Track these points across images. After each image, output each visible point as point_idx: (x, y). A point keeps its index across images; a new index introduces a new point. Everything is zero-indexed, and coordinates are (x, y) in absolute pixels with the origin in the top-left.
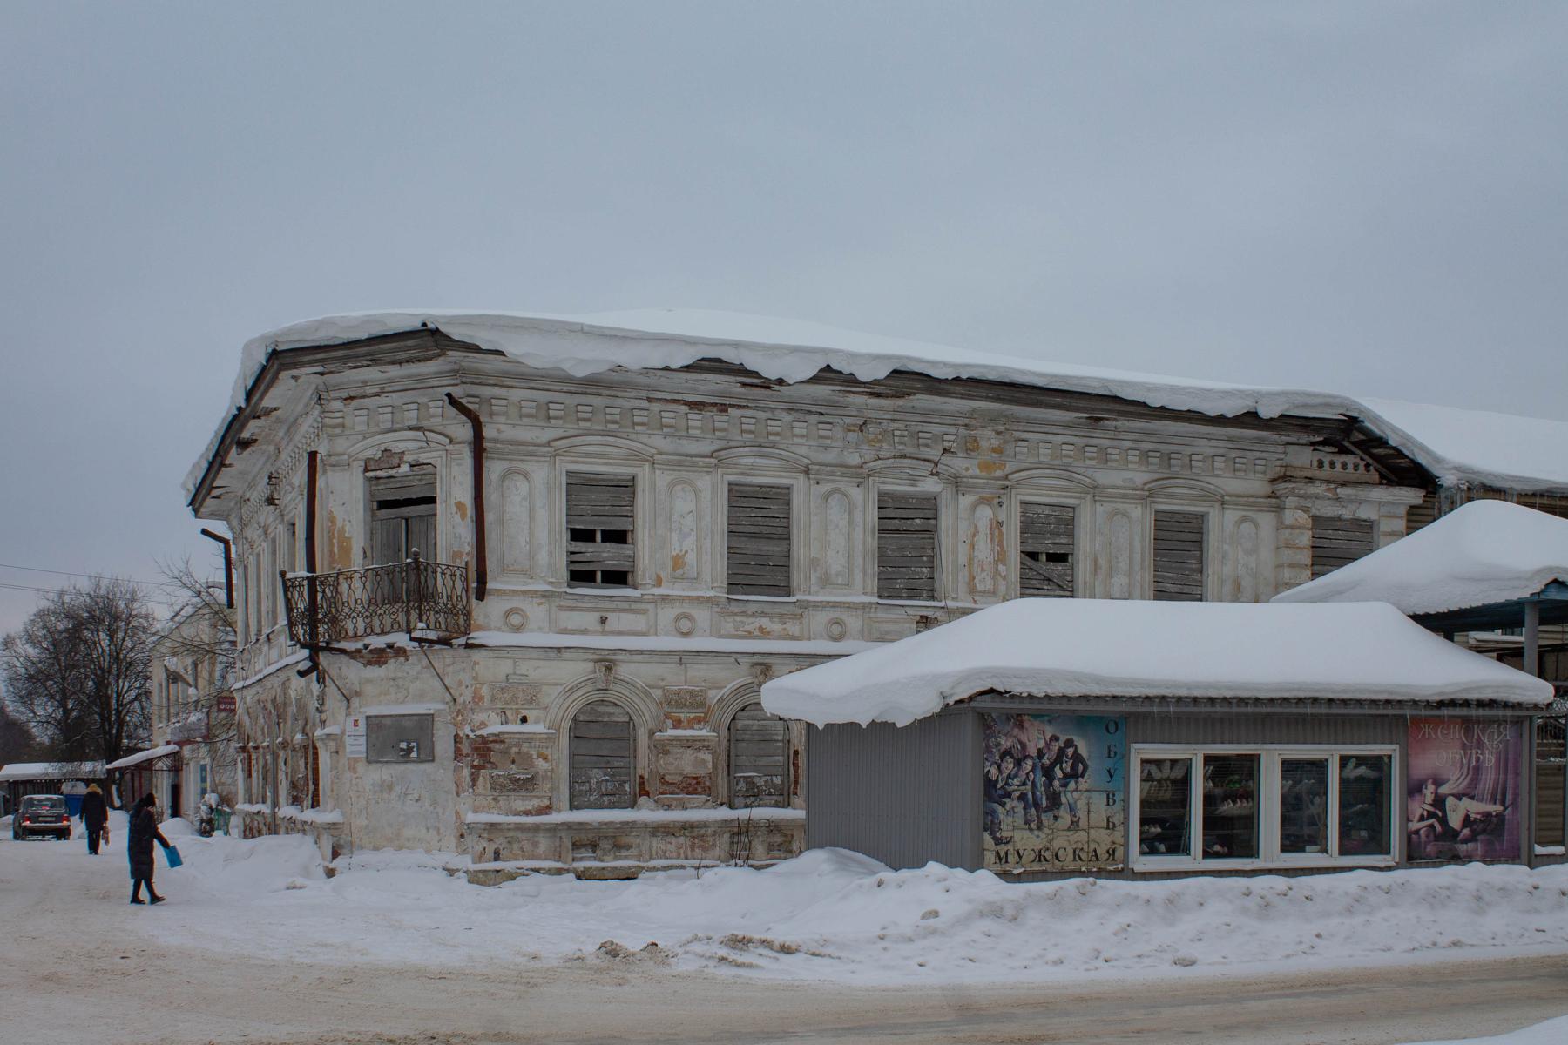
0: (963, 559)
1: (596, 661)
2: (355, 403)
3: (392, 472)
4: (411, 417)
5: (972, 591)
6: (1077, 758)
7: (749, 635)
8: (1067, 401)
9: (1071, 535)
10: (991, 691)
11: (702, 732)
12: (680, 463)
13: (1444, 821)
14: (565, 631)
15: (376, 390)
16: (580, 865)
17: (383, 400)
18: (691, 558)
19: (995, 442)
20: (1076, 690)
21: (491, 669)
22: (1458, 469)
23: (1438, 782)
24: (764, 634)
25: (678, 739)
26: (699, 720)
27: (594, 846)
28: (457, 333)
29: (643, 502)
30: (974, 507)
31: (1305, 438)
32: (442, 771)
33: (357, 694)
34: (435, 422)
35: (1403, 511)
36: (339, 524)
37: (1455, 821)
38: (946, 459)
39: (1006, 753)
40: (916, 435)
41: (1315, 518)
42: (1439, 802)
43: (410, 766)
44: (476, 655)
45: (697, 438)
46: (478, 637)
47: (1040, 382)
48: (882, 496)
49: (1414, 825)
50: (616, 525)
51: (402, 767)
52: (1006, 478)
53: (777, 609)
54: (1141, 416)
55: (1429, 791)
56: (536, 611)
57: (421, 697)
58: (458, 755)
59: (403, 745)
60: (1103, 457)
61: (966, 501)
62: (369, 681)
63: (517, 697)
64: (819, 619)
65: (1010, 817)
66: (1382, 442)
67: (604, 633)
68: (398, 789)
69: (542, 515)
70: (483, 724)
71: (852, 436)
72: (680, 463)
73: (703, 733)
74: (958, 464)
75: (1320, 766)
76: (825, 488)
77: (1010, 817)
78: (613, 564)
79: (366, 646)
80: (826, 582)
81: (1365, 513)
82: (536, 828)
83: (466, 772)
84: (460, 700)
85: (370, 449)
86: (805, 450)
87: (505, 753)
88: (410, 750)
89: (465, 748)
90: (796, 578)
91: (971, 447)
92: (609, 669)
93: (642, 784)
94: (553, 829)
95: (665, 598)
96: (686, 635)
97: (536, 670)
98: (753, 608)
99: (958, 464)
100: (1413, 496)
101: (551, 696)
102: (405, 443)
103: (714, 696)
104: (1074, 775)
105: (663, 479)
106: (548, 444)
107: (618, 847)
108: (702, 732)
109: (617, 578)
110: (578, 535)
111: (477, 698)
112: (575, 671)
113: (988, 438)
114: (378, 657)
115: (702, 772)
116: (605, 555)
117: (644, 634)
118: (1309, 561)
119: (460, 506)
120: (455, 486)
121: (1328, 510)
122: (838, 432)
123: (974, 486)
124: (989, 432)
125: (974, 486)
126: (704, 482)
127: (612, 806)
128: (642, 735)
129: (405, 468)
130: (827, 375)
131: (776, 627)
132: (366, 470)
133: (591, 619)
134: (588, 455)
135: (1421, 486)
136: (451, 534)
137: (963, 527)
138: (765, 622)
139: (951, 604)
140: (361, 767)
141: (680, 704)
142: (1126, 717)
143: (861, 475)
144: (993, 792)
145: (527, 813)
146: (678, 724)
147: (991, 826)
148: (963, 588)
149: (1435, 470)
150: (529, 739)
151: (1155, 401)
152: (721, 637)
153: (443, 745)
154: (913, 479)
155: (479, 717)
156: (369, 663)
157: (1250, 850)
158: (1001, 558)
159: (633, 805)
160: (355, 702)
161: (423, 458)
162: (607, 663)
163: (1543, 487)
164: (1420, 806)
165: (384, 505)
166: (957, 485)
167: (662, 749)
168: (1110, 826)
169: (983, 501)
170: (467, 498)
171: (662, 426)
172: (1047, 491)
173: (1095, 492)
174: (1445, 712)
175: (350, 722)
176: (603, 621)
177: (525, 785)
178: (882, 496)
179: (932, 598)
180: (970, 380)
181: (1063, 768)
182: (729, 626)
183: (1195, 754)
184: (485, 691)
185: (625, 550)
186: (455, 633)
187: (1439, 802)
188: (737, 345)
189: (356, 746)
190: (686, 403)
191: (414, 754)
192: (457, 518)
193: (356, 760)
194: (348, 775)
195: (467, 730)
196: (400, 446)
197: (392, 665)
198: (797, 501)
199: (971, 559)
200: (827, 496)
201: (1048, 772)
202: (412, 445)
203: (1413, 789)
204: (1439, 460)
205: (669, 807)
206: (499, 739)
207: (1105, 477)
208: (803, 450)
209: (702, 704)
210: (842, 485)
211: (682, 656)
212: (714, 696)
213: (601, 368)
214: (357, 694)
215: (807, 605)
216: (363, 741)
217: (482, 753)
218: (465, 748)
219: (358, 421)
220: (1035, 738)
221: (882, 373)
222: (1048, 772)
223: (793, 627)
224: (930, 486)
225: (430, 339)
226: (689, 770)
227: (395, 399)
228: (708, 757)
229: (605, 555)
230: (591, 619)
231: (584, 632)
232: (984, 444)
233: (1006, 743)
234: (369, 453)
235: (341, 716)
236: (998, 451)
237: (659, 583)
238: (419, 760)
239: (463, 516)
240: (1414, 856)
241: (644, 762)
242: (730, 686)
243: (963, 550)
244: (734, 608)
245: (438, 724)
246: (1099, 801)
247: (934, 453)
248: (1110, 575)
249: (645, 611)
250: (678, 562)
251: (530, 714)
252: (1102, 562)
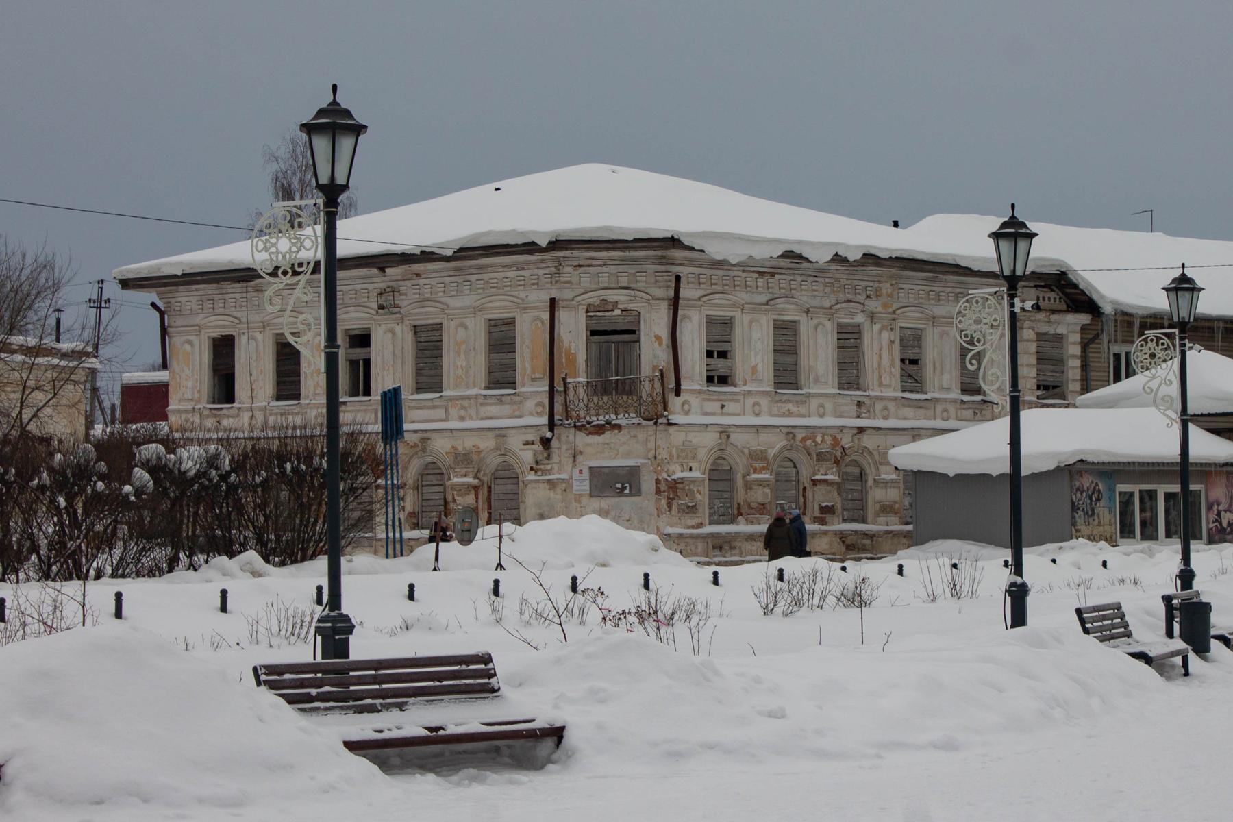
0: (876, 365)
1: (721, 432)
2: (582, 270)
3: (607, 314)
4: (624, 281)
5: (881, 384)
6: (1099, 491)
7: (784, 415)
8: (937, 268)
9: (920, 347)
10: (1082, 460)
11: (765, 476)
12: (754, 309)
13: (1220, 523)
14: (706, 414)
15: (600, 262)
16: (716, 559)
17: (604, 269)
18: (760, 367)
19: (889, 291)
20: (1106, 459)
21: (677, 437)
22: (1113, 302)
23: (1218, 504)
24: (790, 414)
25: (757, 480)
26: (764, 468)
27: (721, 548)
28: (686, 241)
29: (738, 331)
30: (880, 332)
31: (1032, 284)
32: (647, 501)
33: (581, 453)
34: (640, 285)
35: (1079, 328)
36: (566, 343)
37: (1225, 524)
38: (867, 302)
39: (1078, 489)
40: (855, 288)
41: (1038, 334)
42: (1219, 514)
43: (623, 499)
44: (672, 429)
45: (760, 293)
46: (674, 418)
47: (919, 257)
48: (839, 325)
49: (1211, 525)
50: (723, 347)
51: (617, 499)
52: (894, 312)
53: (798, 398)
54: (966, 275)
55: (1215, 507)
56: (695, 402)
57: (628, 455)
58: (658, 492)
59: (619, 486)
60: (938, 299)
61: (876, 327)
62: (588, 445)
63: (686, 455)
64: (814, 403)
65: (1080, 518)
66: (1075, 286)
67: (722, 414)
68: (613, 513)
69: (697, 342)
70: (674, 472)
71: (828, 289)
72: (754, 309)
73: (767, 476)
74: (873, 305)
75: (1132, 494)
76: (815, 321)
77: (1080, 518)
78: (722, 372)
79: (589, 423)
80: (817, 380)
81: (1061, 330)
82: (697, 537)
83: (664, 502)
84: (659, 457)
85: (594, 298)
86: (805, 298)
87: (683, 489)
88: (624, 488)
89: (663, 487)
90: (803, 378)
91: (878, 295)
92: (724, 437)
93: (739, 508)
94: (705, 537)
95: (749, 392)
96: (757, 415)
97: (697, 439)
98: (785, 398)
99: (873, 305)
100: (1084, 319)
101: (702, 454)
102: (621, 297)
103: (771, 453)
104: (1098, 500)
105: (747, 318)
106: (699, 299)
107: (732, 548)
108: (765, 476)
109: (724, 380)
110: (710, 354)
111: (671, 456)
112: (710, 439)
113: (886, 288)
114: (599, 430)
115: (766, 501)
116: (720, 365)
117: (739, 415)
118: (1035, 362)
119: (658, 338)
120: (655, 325)
121: (1044, 328)
122: (821, 288)
123: (880, 318)
124: (888, 285)
125: (880, 318)
126: (764, 320)
127: (724, 523)
128: (739, 476)
129: (617, 312)
130: (838, 258)
131: (793, 408)
132: (587, 312)
133: (715, 406)
134: (715, 305)
135: (1090, 313)
136: (652, 353)
137: (876, 343)
138: (790, 406)
139: (872, 393)
140: (585, 500)
141: (757, 459)
142: (1115, 471)
143: (830, 311)
144: (1074, 508)
145: (693, 527)
146: (755, 471)
147: (1074, 524)
148: (876, 383)
149: (1100, 303)
150: (694, 481)
151: (976, 268)
152: (772, 416)
153: (648, 485)
154: (853, 315)
155: (672, 468)
156: (590, 433)
157: (1157, 539)
158: (892, 365)
159: (733, 521)
160: (580, 458)
161: (631, 306)
162: (725, 432)
163: (1152, 312)
164: (1213, 516)
165: (594, 333)
166: (872, 318)
167: (748, 486)
168: (1111, 524)
169: (883, 328)
170: (665, 334)
171: (746, 286)
172: (911, 319)
173: (934, 320)
174: (1225, 469)
175: (576, 471)
176: (723, 407)
177: (692, 509)
178: (839, 325)
179: (858, 389)
180: (897, 258)
181: (1095, 496)
182: (775, 410)
183: (1136, 489)
184: (674, 452)
185: (728, 362)
186: (656, 416)
187: (1219, 514)
188: (799, 242)
189: (582, 485)
190: (759, 272)
191: (627, 491)
192: (656, 345)
193: (580, 495)
194: (574, 504)
195: (665, 476)
196: (615, 298)
197: (608, 436)
198: (802, 329)
199: (879, 365)
200: (816, 328)
201: (1091, 499)
202: (623, 298)
203: (1210, 508)
204: (1102, 297)
205: (752, 523)
206: (682, 481)
207: (939, 311)
208: (805, 299)
209: (765, 459)
210: (821, 320)
211: (758, 428)
212: (771, 453)
213: (742, 259)
214: (581, 453)
215: (808, 395)
216: (587, 483)
217: (672, 490)
218: (663, 487)
219: (586, 282)
220: (1086, 481)
221: (859, 256)
222: (1091, 499)
223: (803, 410)
224: (860, 319)
225: (673, 242)
226: (760, 500)
227: (613, 269)
228: (768, 491)
229: (720, 365)
230: (715, 406)
231: (713, 414)
232: (884, 292)
233: (1077, 484)
234: (590, 301)
235: (569, 467)
236: (890, 296)
237: (745, 384)
238: (631, 495)
239: (660, 344)
240: (1211, 541)
241: (740, 495)
242: (778, 447)
243: (876, 358)
244: (777, 398)
245: (644, 471)
246: (1107, 511)
247: (861, 298)
248: (942, 374)
249: (737, 401)
250: (754, 370)
251: (694, 465)
252: (938, 365)
